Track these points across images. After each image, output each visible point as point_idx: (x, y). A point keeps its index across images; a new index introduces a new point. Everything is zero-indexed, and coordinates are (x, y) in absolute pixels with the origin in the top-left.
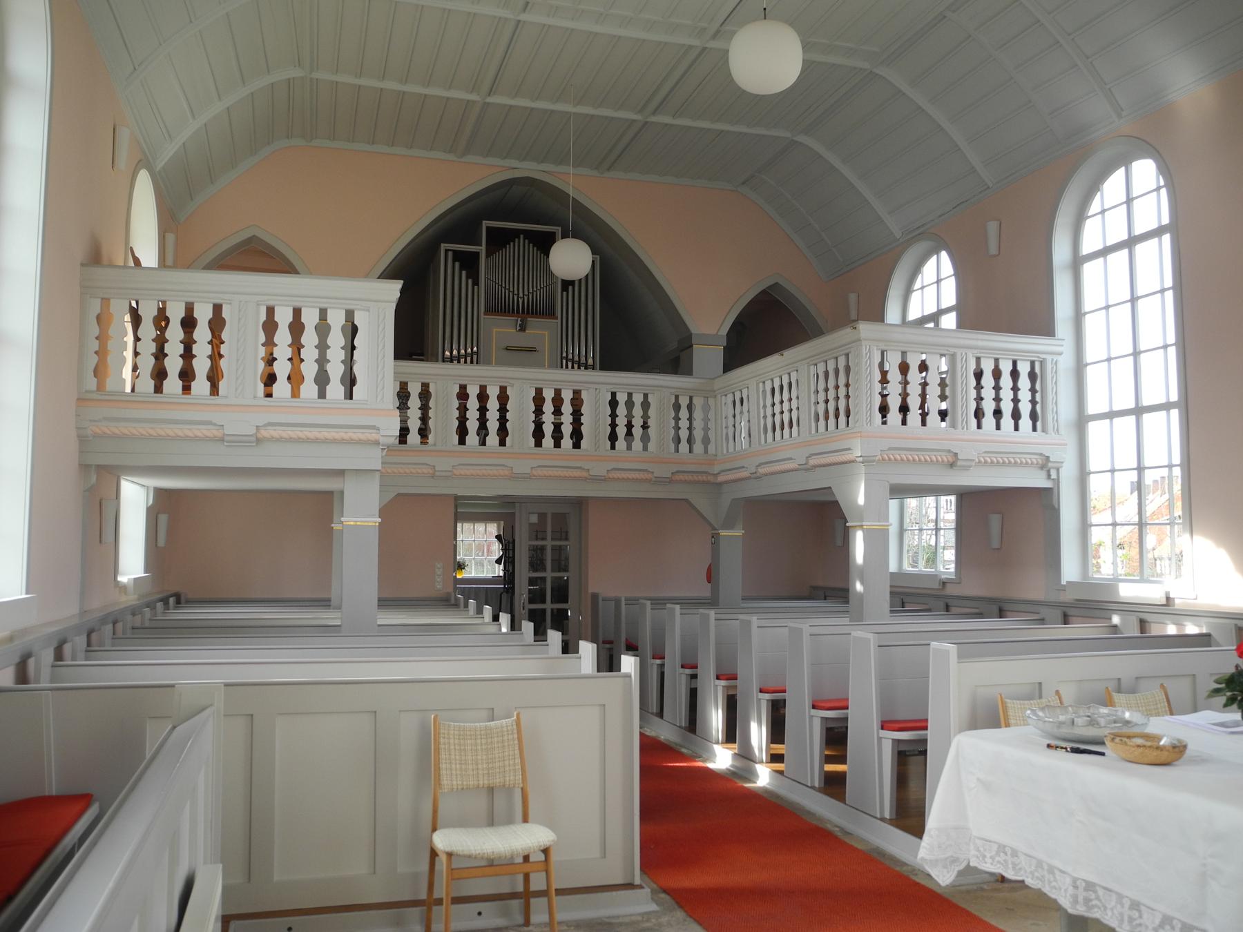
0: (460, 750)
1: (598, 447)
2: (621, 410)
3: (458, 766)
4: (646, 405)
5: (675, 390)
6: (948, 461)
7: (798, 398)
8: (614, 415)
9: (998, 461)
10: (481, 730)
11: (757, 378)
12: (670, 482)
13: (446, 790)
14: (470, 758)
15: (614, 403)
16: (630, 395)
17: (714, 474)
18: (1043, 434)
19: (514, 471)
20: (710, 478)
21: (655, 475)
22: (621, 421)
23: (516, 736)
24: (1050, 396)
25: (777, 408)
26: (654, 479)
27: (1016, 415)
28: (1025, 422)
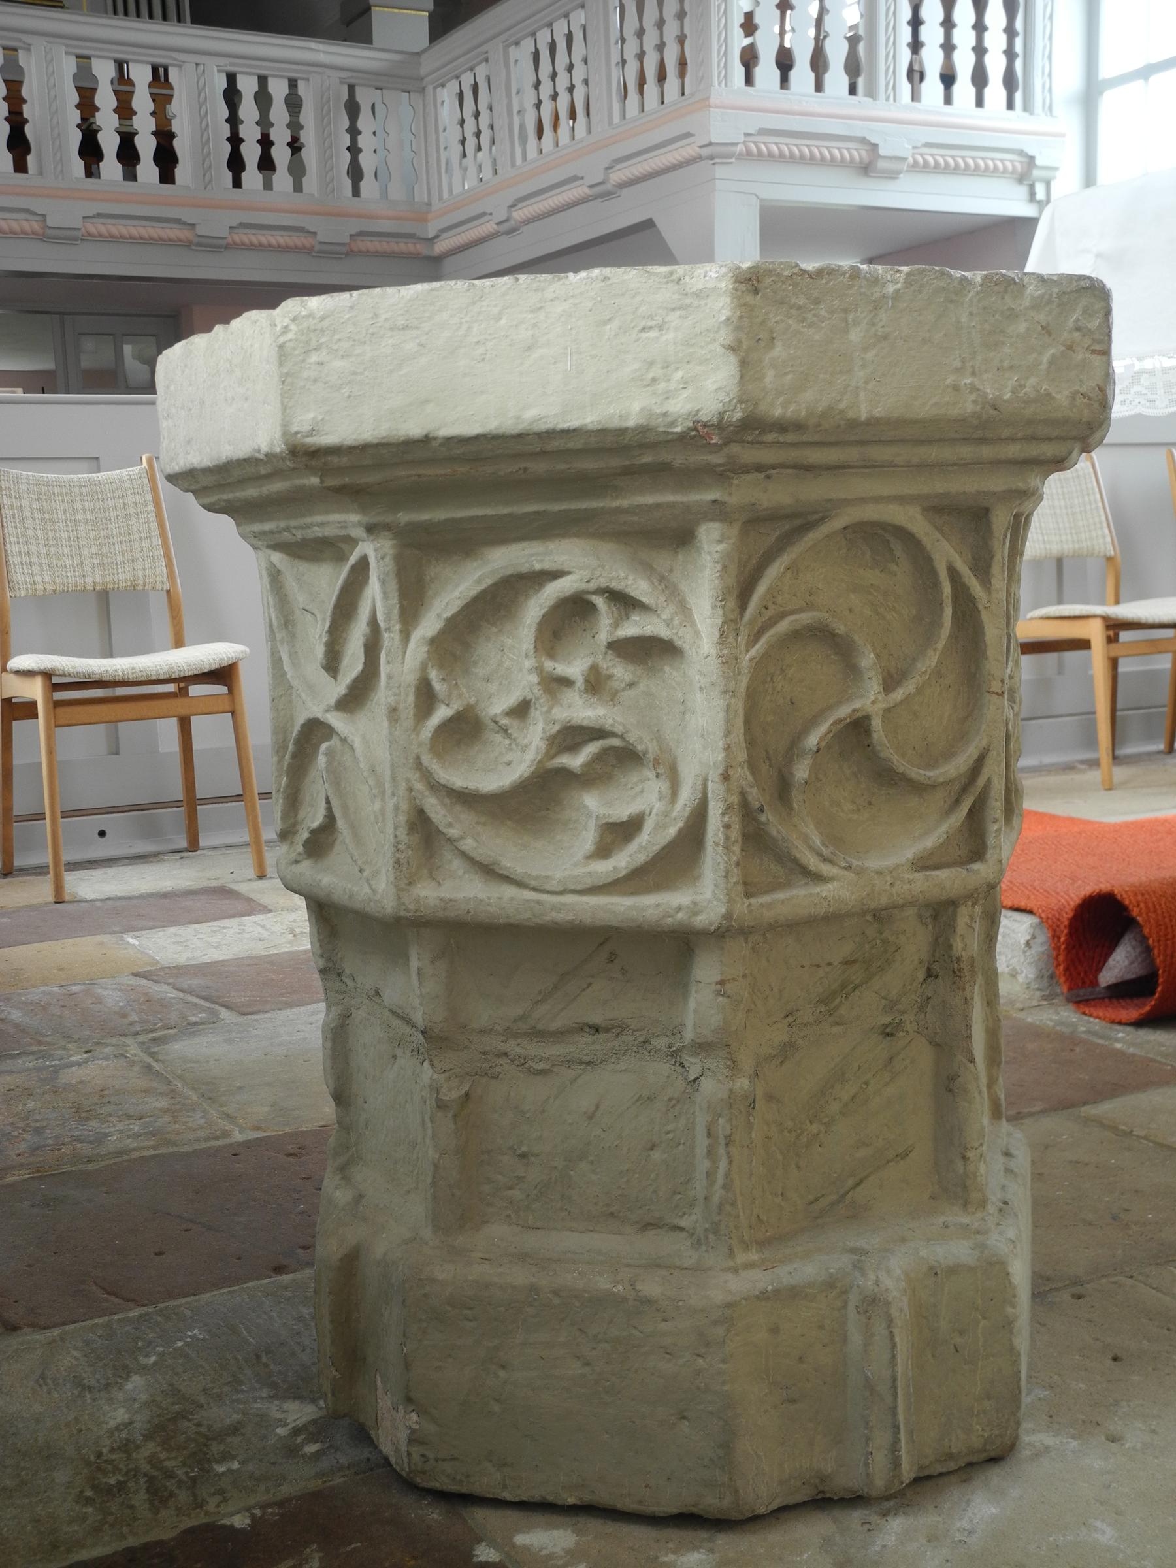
0: (43, 519)
1: (210, 181)
2: (248, 111)
3: (43, 550)
4: (294, 103)
5: (349, 74)
6: (861, 162)
7: (586, 62)
8: (233, 120)
9: (946, 163)
10: (81, 486)
11: (503, 37)
12: (347, 254)
13: (23, 593)
14: (64, 535)
15: (232, 96)
16: (263, 80)
17: (429, 240)
18: (1026, 115)
19: (50, 223)
20: (422, 249)
21: (320, 238)
22: (250, 133)
23: (149, 497)
24: (1039, 61)
25: (546, 89)
26: (317, 247)
27: (980, 78)
28: (995, 91)
